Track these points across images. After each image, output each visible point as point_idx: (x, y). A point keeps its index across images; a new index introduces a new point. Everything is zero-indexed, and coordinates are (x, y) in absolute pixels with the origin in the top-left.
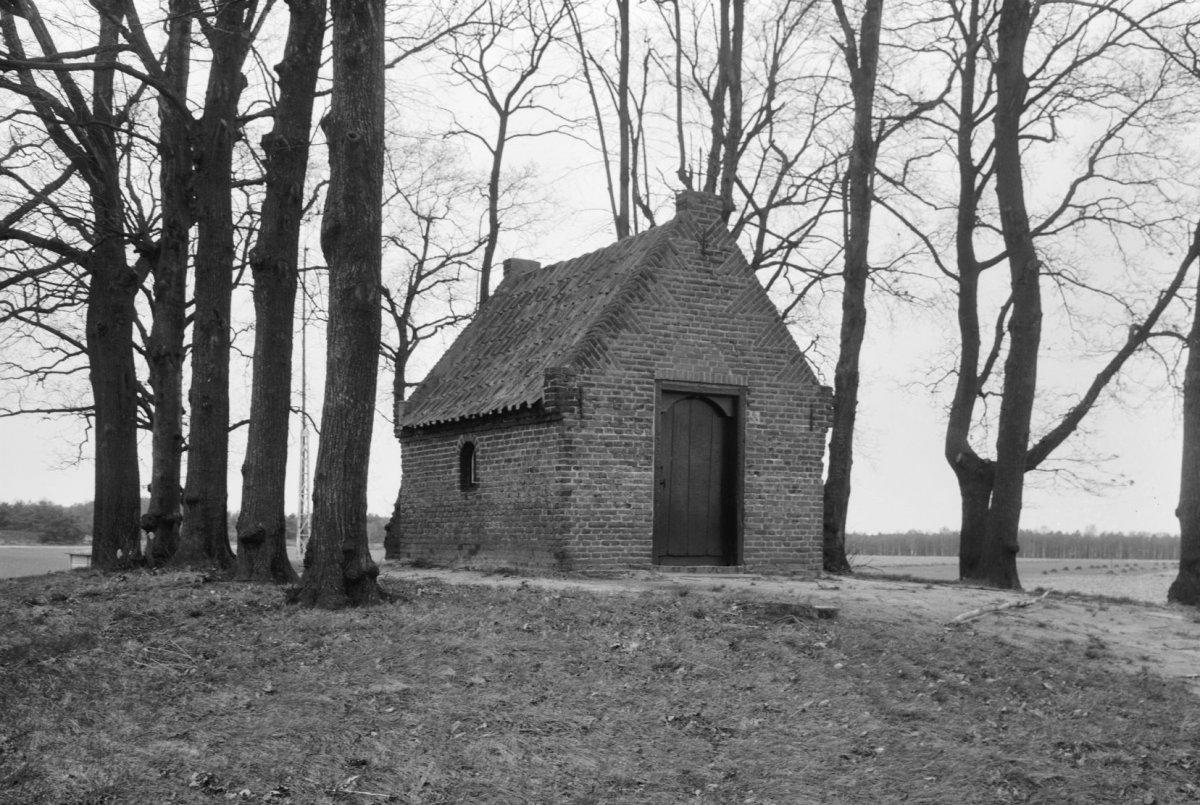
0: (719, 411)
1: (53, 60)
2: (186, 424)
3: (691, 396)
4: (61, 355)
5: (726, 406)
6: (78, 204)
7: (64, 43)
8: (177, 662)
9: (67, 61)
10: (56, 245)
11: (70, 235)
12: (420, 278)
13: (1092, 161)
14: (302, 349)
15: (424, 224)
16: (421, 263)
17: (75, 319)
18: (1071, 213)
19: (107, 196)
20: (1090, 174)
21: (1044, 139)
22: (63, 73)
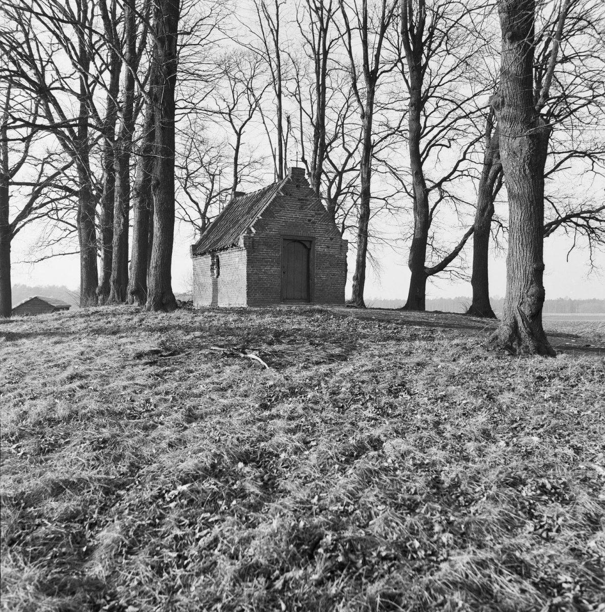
0: (305, 246)
1: (66, 123)
2: (100, 256)
3: (295, 241)
4: (68, 232)
5: (308, 245)
6: (377, 23)
7: (69, 116)
8: (22, 321)
9: (71, 123)
10: (66, 189)
11: (71, 185)
12: (210, 199)
13: (465, 153)
14: (566, 161)
15: (212, 177)
16: (211, 194)
17: (72, 217)
18: (457, 173)
19: (84, 171)
20: (464, 159)
21: (446, 146)
22: (70, 128)
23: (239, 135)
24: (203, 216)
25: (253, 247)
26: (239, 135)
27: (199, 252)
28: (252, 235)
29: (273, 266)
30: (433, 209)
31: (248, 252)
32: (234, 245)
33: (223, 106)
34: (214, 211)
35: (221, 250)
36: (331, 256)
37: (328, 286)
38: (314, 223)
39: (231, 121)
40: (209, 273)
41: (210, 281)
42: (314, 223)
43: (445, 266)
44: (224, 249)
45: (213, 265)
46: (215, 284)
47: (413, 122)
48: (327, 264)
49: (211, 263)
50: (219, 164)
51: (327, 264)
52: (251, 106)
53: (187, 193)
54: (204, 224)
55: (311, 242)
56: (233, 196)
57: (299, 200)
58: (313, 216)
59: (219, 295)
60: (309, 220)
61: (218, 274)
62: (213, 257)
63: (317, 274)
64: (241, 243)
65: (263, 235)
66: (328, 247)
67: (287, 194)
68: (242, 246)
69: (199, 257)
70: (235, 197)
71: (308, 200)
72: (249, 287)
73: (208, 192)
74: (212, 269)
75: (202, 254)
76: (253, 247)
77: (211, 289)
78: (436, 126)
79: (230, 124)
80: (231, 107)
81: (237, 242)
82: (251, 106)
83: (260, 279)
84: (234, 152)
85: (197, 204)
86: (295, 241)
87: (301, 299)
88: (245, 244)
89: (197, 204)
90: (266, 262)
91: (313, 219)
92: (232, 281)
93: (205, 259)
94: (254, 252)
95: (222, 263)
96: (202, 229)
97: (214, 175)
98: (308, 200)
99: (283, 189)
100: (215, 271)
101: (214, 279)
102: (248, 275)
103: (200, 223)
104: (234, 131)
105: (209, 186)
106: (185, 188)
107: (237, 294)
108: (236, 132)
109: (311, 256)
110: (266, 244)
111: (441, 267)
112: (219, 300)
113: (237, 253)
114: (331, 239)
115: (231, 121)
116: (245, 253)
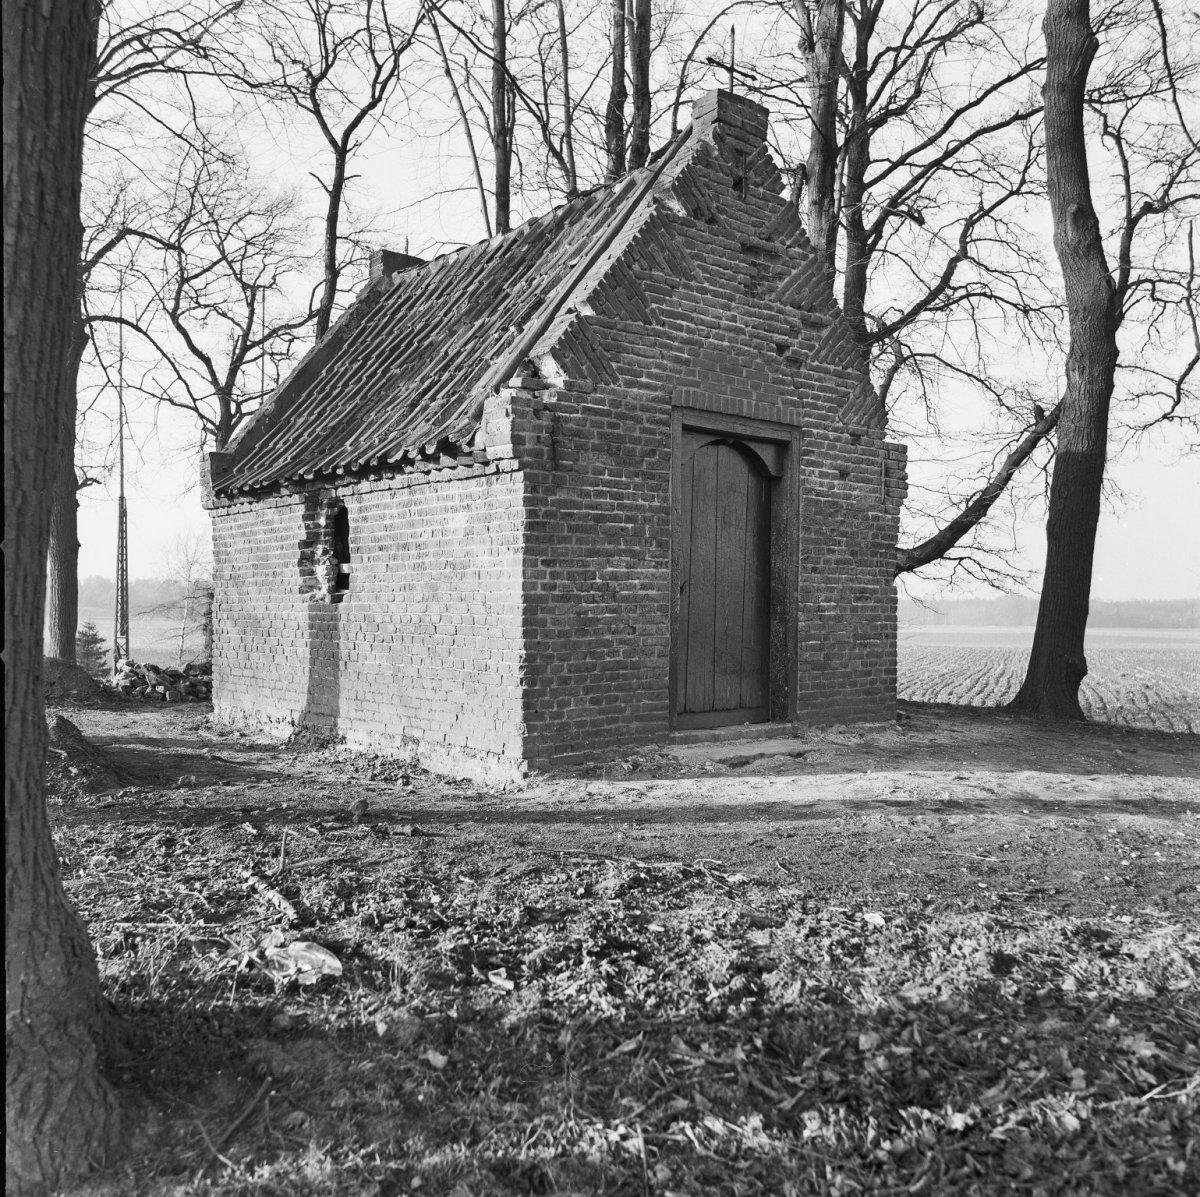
5: (767, 455)
12: (245, 349)
23: (341, 152)
24: (224, 393)
25: (555, 456)
26: (341, 152)
27: (248, 480)
28: (547, 398)
29: (638, 557)
30: (885, 388)
31: (532, 484)
32: (448, 448)
33: (297, 77)
34: (259, 380)
35: (363, 472)
36: (856, 512)
37: (841, 643)
38: (795, 361)
39: (317, 113)
40: (293, 576)
41: (299, 612)
42: (795, 361)
43: (951, 544)
44: (383, 467)
45: (310, 542)
46: (325, 632)
47: (1064, 23)
48: (841, 551)
49: (302, 535)
50: (268, 260)
51: (841, 551)
52: (379, 68)
53: (180, 328)
54: (227, 415)
55: (782, 447)
56: (379, 267)
57: (748, 249)
58: (793, 332)
59: (347, 683)
60: (781, 348)
61: (341, 582)
62: (312, 505)
63: (807, 591)
64: (496, 434)
65: (601, 398)
66: (843, 474)
67: (696, 212)
68: (505, 448)
69: (243, 505)
70: (388, 271)
71: (773, 255)
72: (533, 669)
73: (238, 332)
74: (306, 560)
75: (258, 494)
76: (555, 456)
77: (304, 652)
78: (902, 162)
79: (313, 116)
80: (316, 71)
81: (470, 431)
82: (379, 68)
83: (584, 624)
84: (327, 200)
85: (207, 361)
86: (721, 439)
87: (741, 707)
88: (516, 440)
89: (207, 361)
90: (613, 537)
91: (795, 344)
92: (425, 629)
93: (270, 514)
94: (559, 484)
95: (361, 530)
96: (224, 428)
97: (254, 288)
98: (773, 255)
99: (682, 188)
100: (321, 571)
101: (315, 605)
102: (532, 606)
103: (212, 408)
104: (326, 141)
105: (241, 312)
106: (174, 316)
107: (459, 694)
108: (333, 141)
109: (785, 511)
110: (612, 446)
111: (936, 548)
112: (345, 706)
113: (456, 488)
114: (856, 438)
115: (317, 113)
116: (511, 492)
